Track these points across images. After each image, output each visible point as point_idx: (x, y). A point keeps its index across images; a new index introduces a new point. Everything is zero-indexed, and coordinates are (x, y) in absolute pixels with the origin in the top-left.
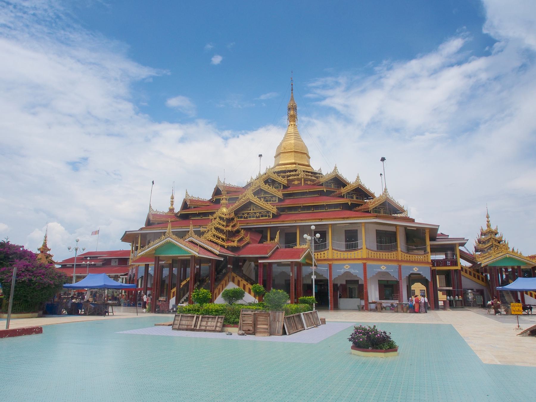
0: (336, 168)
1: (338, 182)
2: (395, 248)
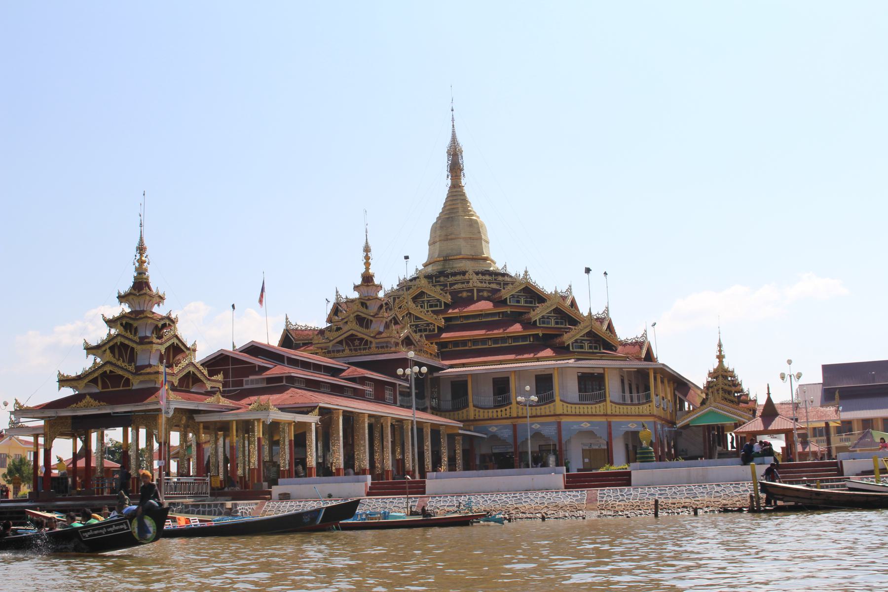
0: (526, 272)
1: (532, 294)
2: (602, 398)
